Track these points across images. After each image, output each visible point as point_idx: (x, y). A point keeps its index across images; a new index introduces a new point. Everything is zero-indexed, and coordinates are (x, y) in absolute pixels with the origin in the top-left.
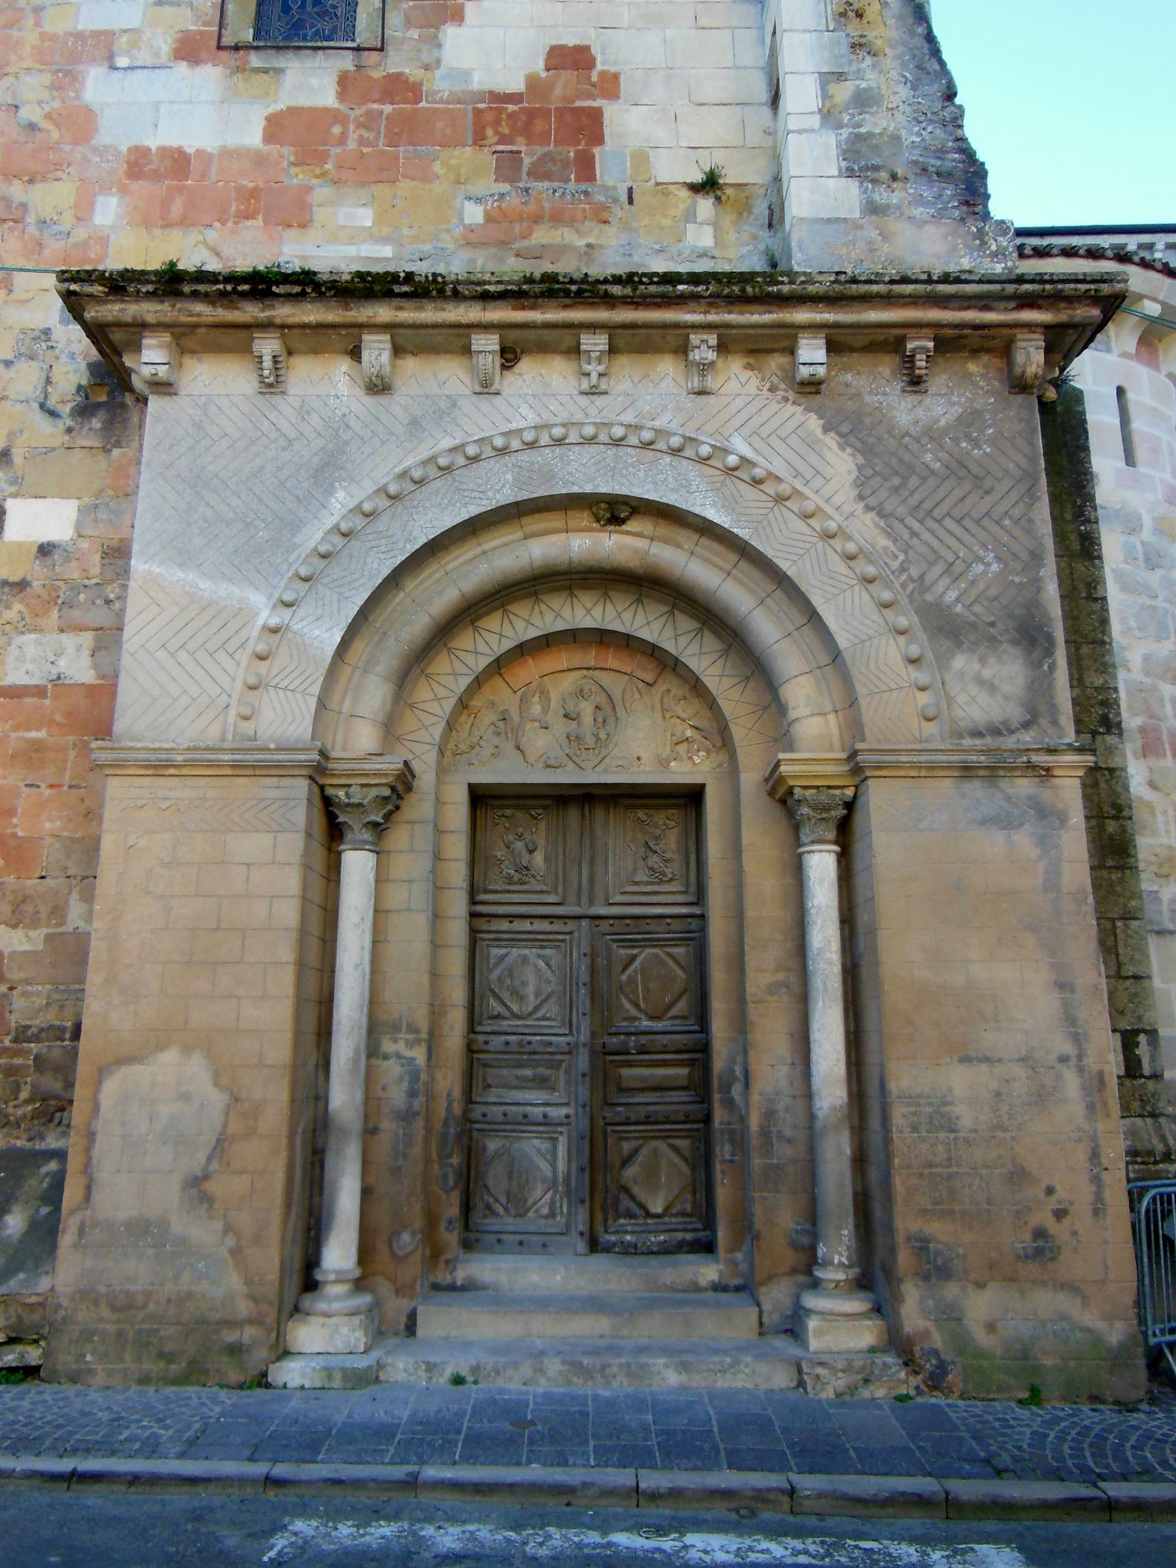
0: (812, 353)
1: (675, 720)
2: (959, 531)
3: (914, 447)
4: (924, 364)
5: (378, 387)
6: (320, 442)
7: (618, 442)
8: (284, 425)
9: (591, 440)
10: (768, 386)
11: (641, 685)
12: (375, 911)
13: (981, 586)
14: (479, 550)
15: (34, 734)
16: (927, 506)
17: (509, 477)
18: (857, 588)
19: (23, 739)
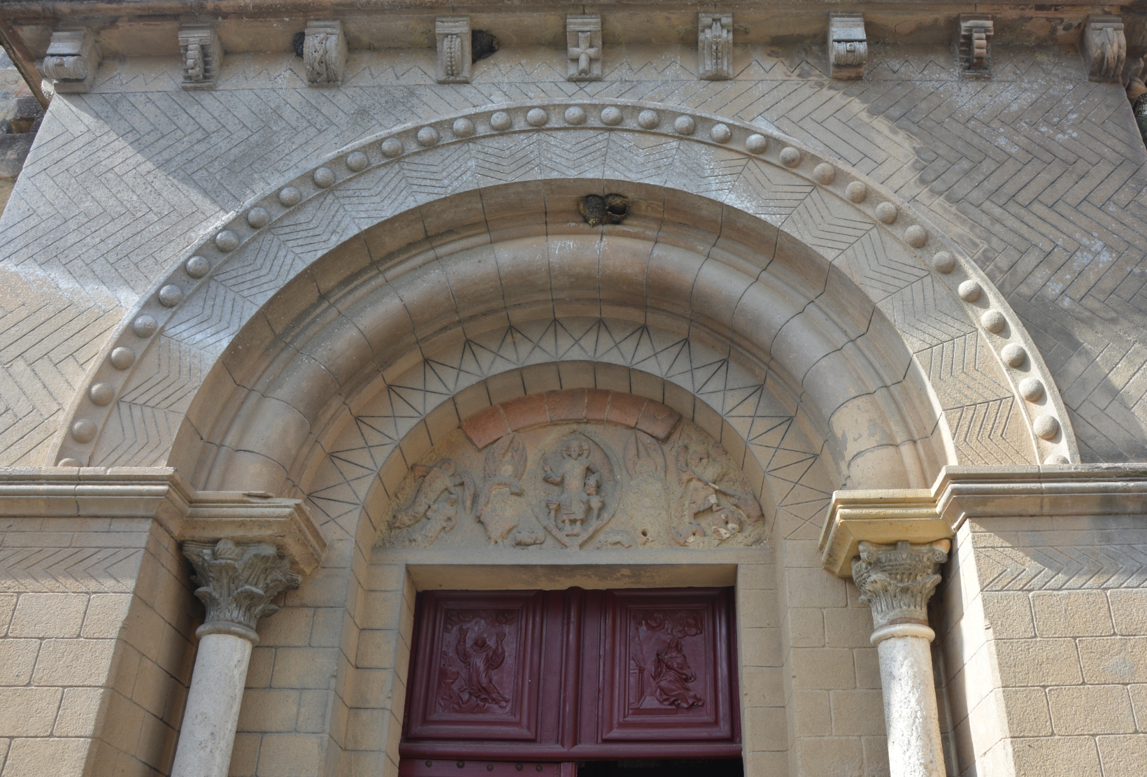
2: (1052, 217)
5: (324, 79)
6: (244, 134)
10: (797, 72)
11: (649, 440)
12: (240, 732)
13: (1092, 278)
14: (431, 254)
16: (1009, 189)
17: (472, 163)
18: (928, 280)
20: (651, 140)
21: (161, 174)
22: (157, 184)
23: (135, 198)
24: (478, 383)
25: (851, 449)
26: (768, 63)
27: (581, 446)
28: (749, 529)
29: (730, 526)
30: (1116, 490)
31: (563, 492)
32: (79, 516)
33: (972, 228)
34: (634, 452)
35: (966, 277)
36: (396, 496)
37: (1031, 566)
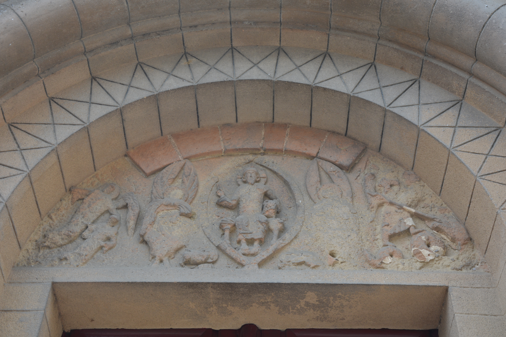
11: (333, 168)
24: (149, 97)
27: (257, 173)
28: (454, 255)
29: (433, 248)
31: (238, 215)
34: (317, 178)
36: (50, 217)
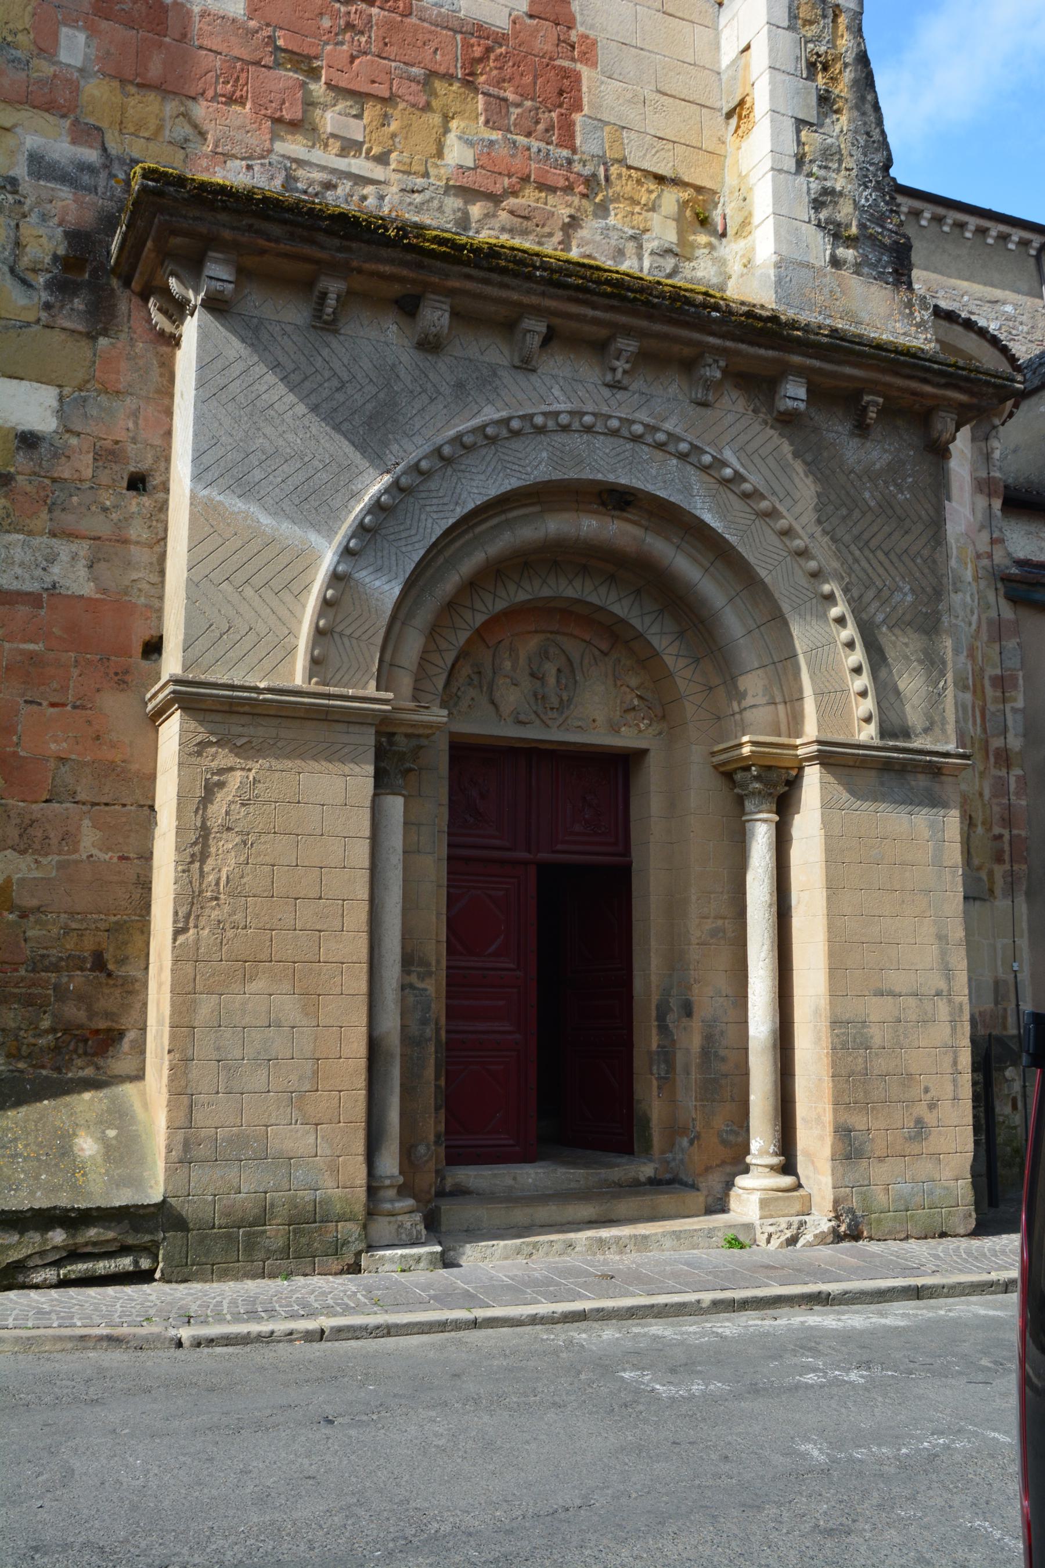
0: (794, 392)
1: (624, 688)
3: (857, 483)
4: (874, 415)
5: (430, 345)
6: (371, 389)
7: (636, 439)
8: (336, 365)
9: (614, 433)
11: (597, 653)
14: (503, 517)
15: (31, 647)
16: (866, 536)
17: (544, 454)
19: (22, 652)
20: (659, 455)
21: (312, 417)
22: (314, 430)
23: (299, 441)
25: (749, 701)
26: (735, 394)
30: (893, 758)
32: (326, 720)
33: (842, 564)
35: (836, 605)
37: (846, 795)
